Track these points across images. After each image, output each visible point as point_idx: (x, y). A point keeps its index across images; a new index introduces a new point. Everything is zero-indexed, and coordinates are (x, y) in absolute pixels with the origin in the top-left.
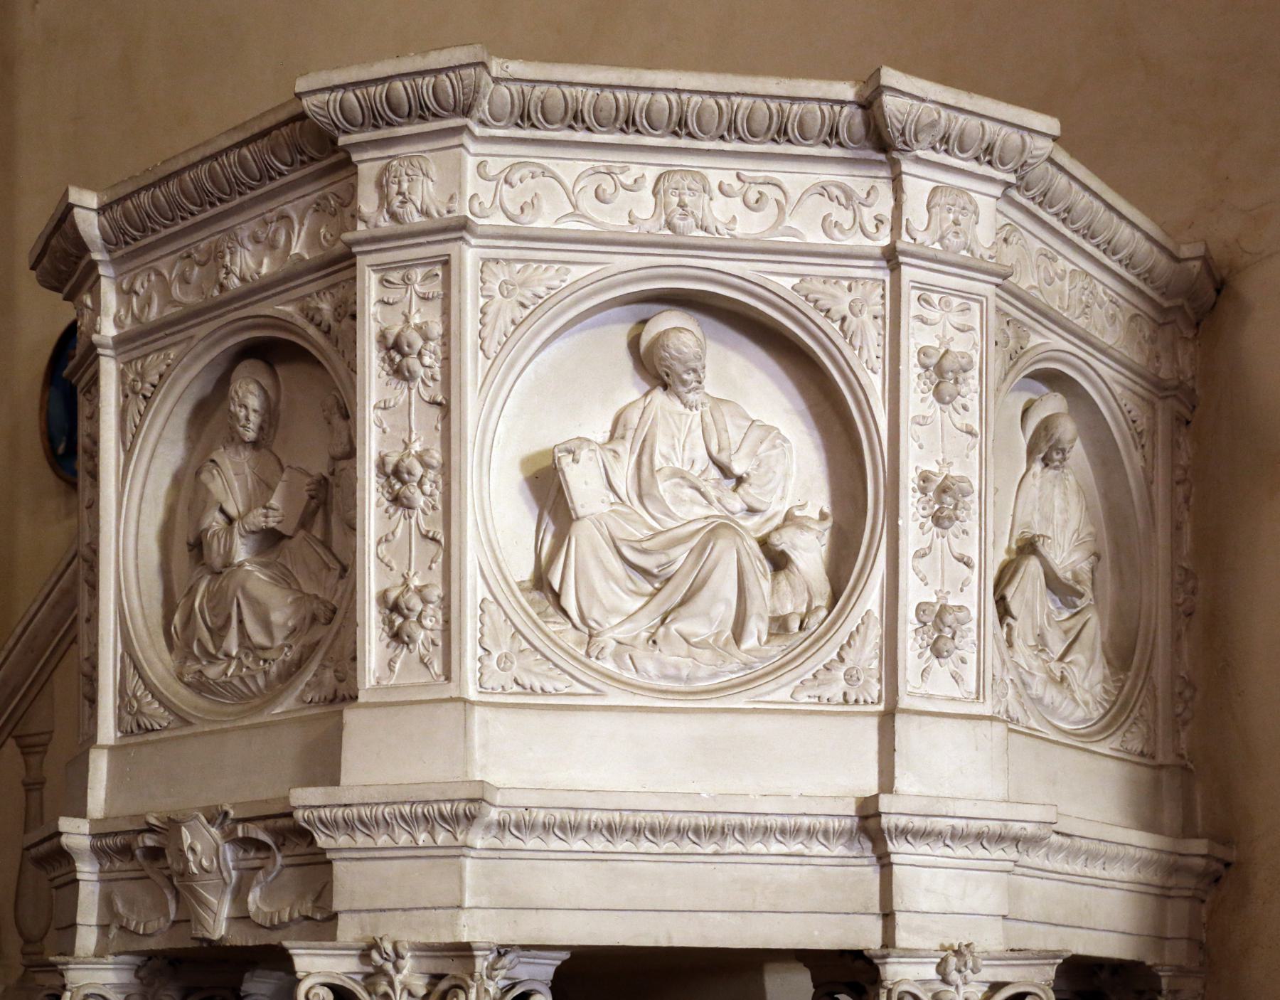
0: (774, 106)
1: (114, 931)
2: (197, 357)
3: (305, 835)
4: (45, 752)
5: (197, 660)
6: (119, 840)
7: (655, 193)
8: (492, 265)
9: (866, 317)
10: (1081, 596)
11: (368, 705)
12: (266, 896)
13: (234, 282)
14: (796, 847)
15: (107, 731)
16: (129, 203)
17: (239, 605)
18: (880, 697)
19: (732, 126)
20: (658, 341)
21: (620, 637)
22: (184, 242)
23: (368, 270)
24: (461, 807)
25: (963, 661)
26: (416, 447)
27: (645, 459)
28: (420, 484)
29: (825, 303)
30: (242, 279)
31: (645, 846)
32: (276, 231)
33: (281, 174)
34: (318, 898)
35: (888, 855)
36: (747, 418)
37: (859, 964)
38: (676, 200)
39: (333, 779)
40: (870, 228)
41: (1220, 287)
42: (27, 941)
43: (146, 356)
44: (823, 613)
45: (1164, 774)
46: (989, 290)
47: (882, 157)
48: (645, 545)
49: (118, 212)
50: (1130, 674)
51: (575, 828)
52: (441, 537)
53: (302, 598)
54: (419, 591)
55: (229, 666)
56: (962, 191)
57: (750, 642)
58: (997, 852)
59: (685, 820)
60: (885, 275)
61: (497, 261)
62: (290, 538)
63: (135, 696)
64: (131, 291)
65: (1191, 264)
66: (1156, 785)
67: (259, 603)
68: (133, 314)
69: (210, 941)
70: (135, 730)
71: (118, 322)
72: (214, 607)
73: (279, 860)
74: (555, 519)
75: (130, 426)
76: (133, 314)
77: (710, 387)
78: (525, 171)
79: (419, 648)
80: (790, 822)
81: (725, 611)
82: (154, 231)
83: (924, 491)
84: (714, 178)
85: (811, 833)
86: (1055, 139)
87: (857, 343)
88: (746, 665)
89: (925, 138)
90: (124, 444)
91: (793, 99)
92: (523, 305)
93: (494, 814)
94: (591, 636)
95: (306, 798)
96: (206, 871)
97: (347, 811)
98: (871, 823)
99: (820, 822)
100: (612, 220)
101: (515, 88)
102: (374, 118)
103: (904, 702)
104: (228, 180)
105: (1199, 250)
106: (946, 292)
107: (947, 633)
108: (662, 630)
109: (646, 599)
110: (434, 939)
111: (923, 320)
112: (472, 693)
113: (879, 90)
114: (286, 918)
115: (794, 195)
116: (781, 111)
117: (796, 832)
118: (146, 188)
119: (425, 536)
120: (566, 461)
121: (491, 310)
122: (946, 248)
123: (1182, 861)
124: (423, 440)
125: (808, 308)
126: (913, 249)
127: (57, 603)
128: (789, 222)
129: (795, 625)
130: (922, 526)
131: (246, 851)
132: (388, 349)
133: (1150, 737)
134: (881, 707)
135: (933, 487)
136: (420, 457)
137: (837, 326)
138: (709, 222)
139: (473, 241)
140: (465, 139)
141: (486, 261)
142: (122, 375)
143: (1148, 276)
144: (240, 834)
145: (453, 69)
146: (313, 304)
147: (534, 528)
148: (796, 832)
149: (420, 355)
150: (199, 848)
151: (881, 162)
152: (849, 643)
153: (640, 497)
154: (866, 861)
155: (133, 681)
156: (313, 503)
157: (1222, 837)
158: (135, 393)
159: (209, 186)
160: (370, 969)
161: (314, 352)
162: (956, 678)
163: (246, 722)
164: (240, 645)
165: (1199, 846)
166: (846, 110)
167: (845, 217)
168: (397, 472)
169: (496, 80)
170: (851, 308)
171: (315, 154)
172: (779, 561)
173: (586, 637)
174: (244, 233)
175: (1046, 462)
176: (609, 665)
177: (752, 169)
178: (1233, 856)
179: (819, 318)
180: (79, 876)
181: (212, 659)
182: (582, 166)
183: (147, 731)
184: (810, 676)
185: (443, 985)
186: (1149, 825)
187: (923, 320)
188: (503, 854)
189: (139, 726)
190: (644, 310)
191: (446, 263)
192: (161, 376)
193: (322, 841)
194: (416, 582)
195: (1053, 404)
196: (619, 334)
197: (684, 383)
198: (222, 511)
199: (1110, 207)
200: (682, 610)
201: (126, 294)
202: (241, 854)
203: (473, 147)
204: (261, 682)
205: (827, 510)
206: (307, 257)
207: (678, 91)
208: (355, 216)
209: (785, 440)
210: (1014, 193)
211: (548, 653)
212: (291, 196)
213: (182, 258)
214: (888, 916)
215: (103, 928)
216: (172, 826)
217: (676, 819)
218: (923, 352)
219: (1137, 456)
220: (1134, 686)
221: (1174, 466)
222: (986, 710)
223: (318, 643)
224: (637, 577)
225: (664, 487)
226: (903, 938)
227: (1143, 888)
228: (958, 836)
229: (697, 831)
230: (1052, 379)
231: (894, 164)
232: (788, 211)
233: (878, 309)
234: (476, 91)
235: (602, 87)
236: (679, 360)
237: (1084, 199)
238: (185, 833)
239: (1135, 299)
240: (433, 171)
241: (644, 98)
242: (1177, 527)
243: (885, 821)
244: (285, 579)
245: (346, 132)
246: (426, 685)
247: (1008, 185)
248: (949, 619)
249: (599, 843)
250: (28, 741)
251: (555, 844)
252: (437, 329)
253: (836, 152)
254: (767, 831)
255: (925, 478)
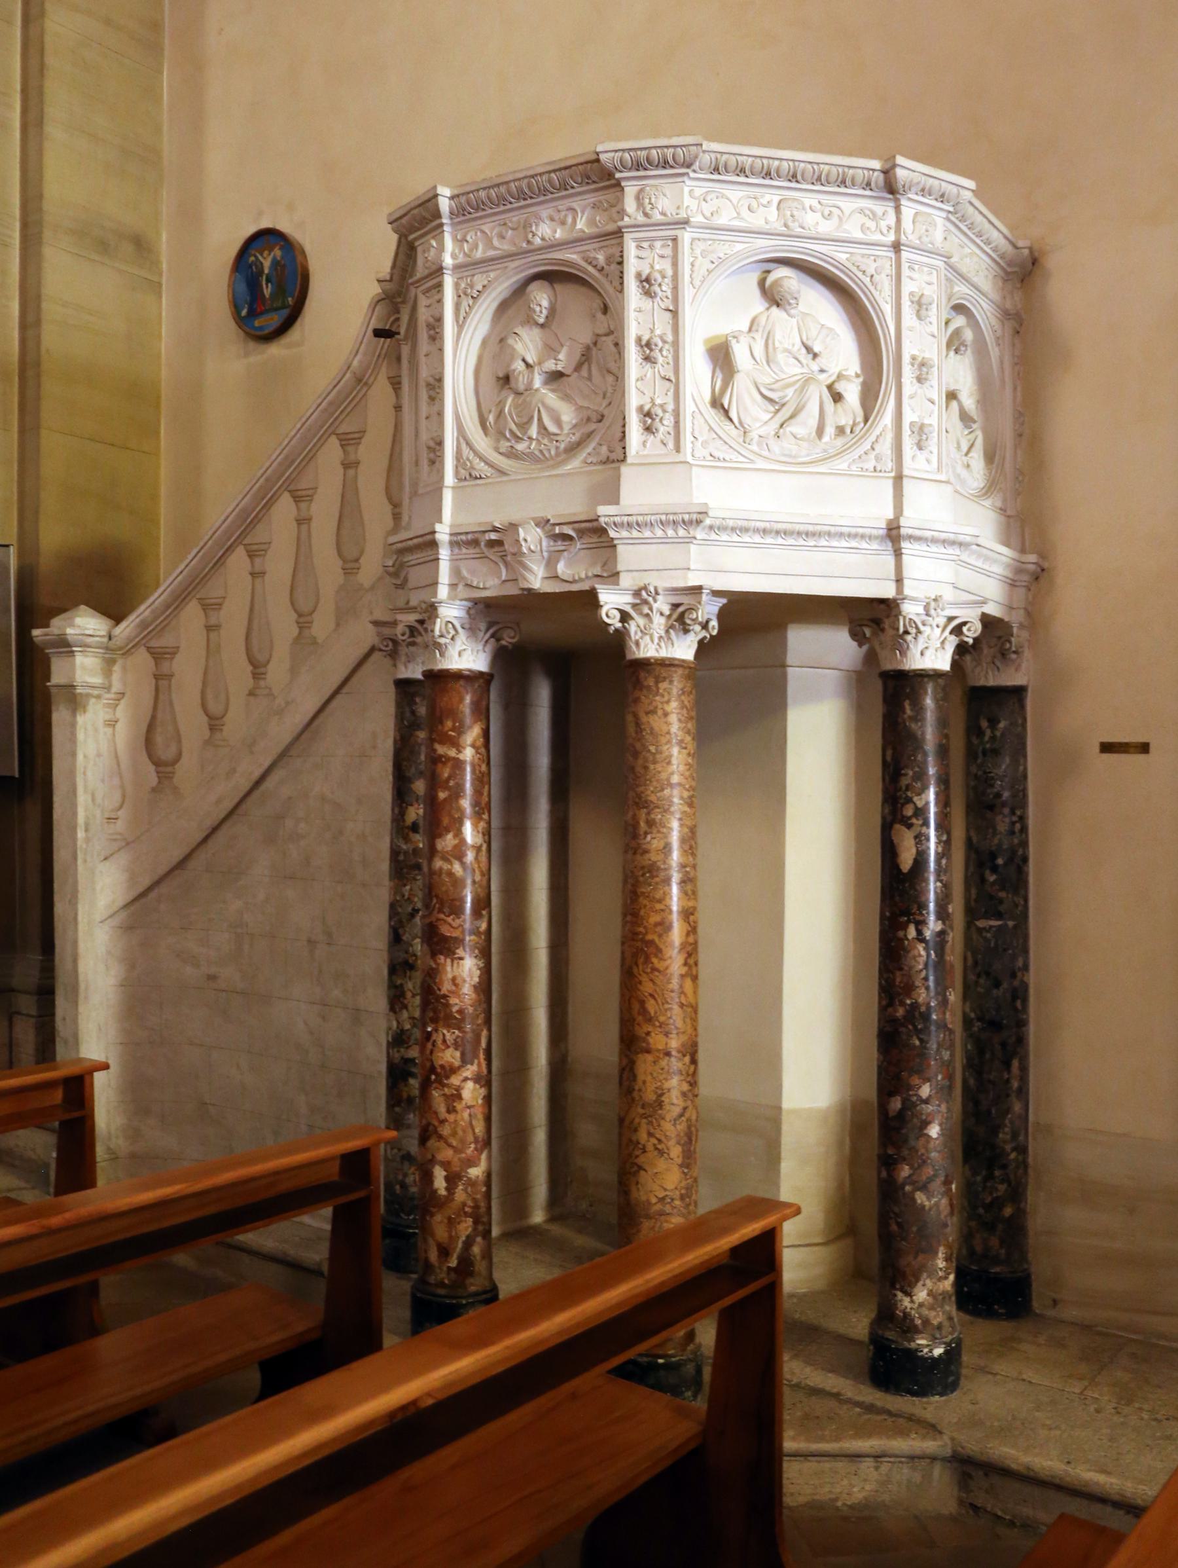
0: (840, 170)
1: (460, 587)
2: (508, 278)
3: (602, 531)
4: (311, 500)
5: (508, 440)
6: (470, 537)
7: (778, 208)
8: (697, 241)
9: (883, 276)
10: (975, 422)
11: (632, 464)
12: (569, 564)
13: (538, 241)
14: (854, 544)
15: (449, 478)
16: (471, 195)
17: (539, 411)
18: (892, 470)
19: (819, 179)
20: (776, 282)
21: (761, 434)
22: (503, 216)
23: (630, 241)
24: (694, 517)
25: (931, 452)
26: (658, 332)
27: (770, 342)
28: (661, 350)
29: (863, 267)
30: (543, 239)
31: (780, 541)
32: (566, 216)
33: (573, 187)
34: (604, 564)
35: (900, 549)
36: (819, 323)
37: (882, 606)
38: (789, 213)
39: (616, 501)
40: (885, 231)
41: (1035, 262)
42: (300, 615)
43: (473, 275)
44: (862, 425)
45: (1011, 520)
46: (941, 264)
47: (891, 196)
48: (773, 386)
49: (463, 199)
50: (994, 465)
51: (746, 530)
52: (673, 379)
53: (580, 408)
54: (662, 406)
55: (531, 444)
56: (930, 215)
57: (826, 439)
58: (950, 550)
59: (802, 528)
60: (892, 255)
61: (699, 240)
62: (568, 376)
63: (468, 459)
64: (464, 240)
65: (1023, 250)
66: (1008, 526)
67: (553, 410)
68: (464, 253)
69: (529, 590)
70: (468, 477)
71: (454, 256)
72: (520, 412)
73: (579, 546)
74: (722, 370)
75: (462, 314)
76: (464, 253)
77: (801, 308)
78: (713, 196)
79: (660, 435)
80: (853, 531)
81: (813, 422)
82: (484, 210)
83: (913, 365)
84: (807, 202)
85: (863, 537)
86: (973, 191)
87: (879, 288)
88: (825, 451)
89: (914, 190)
90: (457, 322)
91: (850, 167)
92: (713, 262)
93: (708, 522)
94: (745, 433)
95: (605, 511)
96: (533, 552)
97: (630, 518)
98: (894, 532)
99: (867, 531)
100: (756, 221)
101: (713, 156)
102: (638, 166)
103: (906, 472)
104: (539, 188)
105: (1027, 243)
106: (922, 264)
107: (924, 437)
108: (782, 430)
109: (772, 415)
110: (675, 585)
111: (911, 279)
112: (689, 459)
113: (894, 166)
114: (583, 576)
115: (847, 213)
116: (844, 172)
117: (856, 536)
118: (484, 189)
119: (664, 378)
120: (734, 342)
121: (697, 264)
122: (921, 242)
123: (1024, 566)
124: (662, 326)
125: (854, 269)
126: (907, 243)
127: (326, 410)
128: (846, 227)
129: (848, 431)
130: (911, 382)
131: (555, 541)
132: (642, 282)
133: (1004, 501)
134: (893, 474)
135: (917, 362)
136: (661, 338)
137: (868, 279)
138: (805, 225)
139: (688, 229)
140: (685, 179)
141: (693, 240)
142: (456, 285)
143: (1002, 257)
144: (557, 531)
145: (684, 146)
146: (592, 255)
147: (710, 375)
148: (856, 536)
149: (660, 285)
150: (529, 539)
151: (890, 199)
152: (876, 440)
153: (768, 362)
154: (888, 553)
155: (465, 450)
156: (584, 358)
157: (1042, 556)
158: (465, 294)
159: (526, 190)
160: (638, 601)
161: (591, 281)
162: (928, 461)
163: (547, 474)
164: (538, 433)
165: (1032, 558)
166: (876, 173)
167: (871, 224)
168: (648, 345)
169: (704, 152)
170: (876, 270)
171: (595, 179)
172: (837, 397)
173: (742, 433)
174: (544, 214)
175: (957, 351)
176: (754, 447)
177: (828, 200)
178: (1046, 565)
179: (860, 274)
180: (440, 557)
181: (518, 439)
182: (742, 194)
183: (476, 478)
184: (857, 457)
185: (681, 609)
186: (1007, 544)
187: (911, 279)
188: (709, 543)
189: (470, 475)
190: (771, 266)
191: (675, 240)
192: (484, 286)
193: (612, 534)
194: (658, 401)
195: (960, 321)
196: (754, 278)
197: (790, 304)
198: (524, 360)
199: (990, 222)
200: (792, 421)
201: (460, 241)
202: (552, 543)
203: (688, 182)
204: (553, 452)
205: (859, 372)
206: (586, 231)
207: (793, 161)
208: (622, 213)
209: (838, 335)
210: (950, 216)
211: (727, 440)
212: (576, 199)
213: (500, 225)
214: (899, 581)
215: (453, 586)
216: (513, 527)
217: (798, 527)
218: (912, 294)
219: (997, 349)
220: (996, 472)
221: (1013, 356)
222: (943, 477)
223: (592, 432)
224: (766, 402)
225: (781, 357)
226: (907, 591)
227: (1008, 581)
228: (934, 541)
229: (807, 534)
230: (959, 309)
231: (897, 201)
232: (844, 220)
233: (889, 272)
234: (696, 157)
235: (756, 157)
236: (789, 293)
237: (980, 218)
238: (521, 530)
239: (995, 267)
240: (668, 193)
241: (776, 163)
242: (1015, 389)
243: (903, 531)
244: (566, 397)
245: (621, 172)
246: (666, 455)
247: (950, 212)
248: (926, 430)
249: (757, 538)
250: (299, 493)
251: (735, 538)
252: (669, 273)
253: (868, 193)
254: (841, 535)
255: (914, 358)
